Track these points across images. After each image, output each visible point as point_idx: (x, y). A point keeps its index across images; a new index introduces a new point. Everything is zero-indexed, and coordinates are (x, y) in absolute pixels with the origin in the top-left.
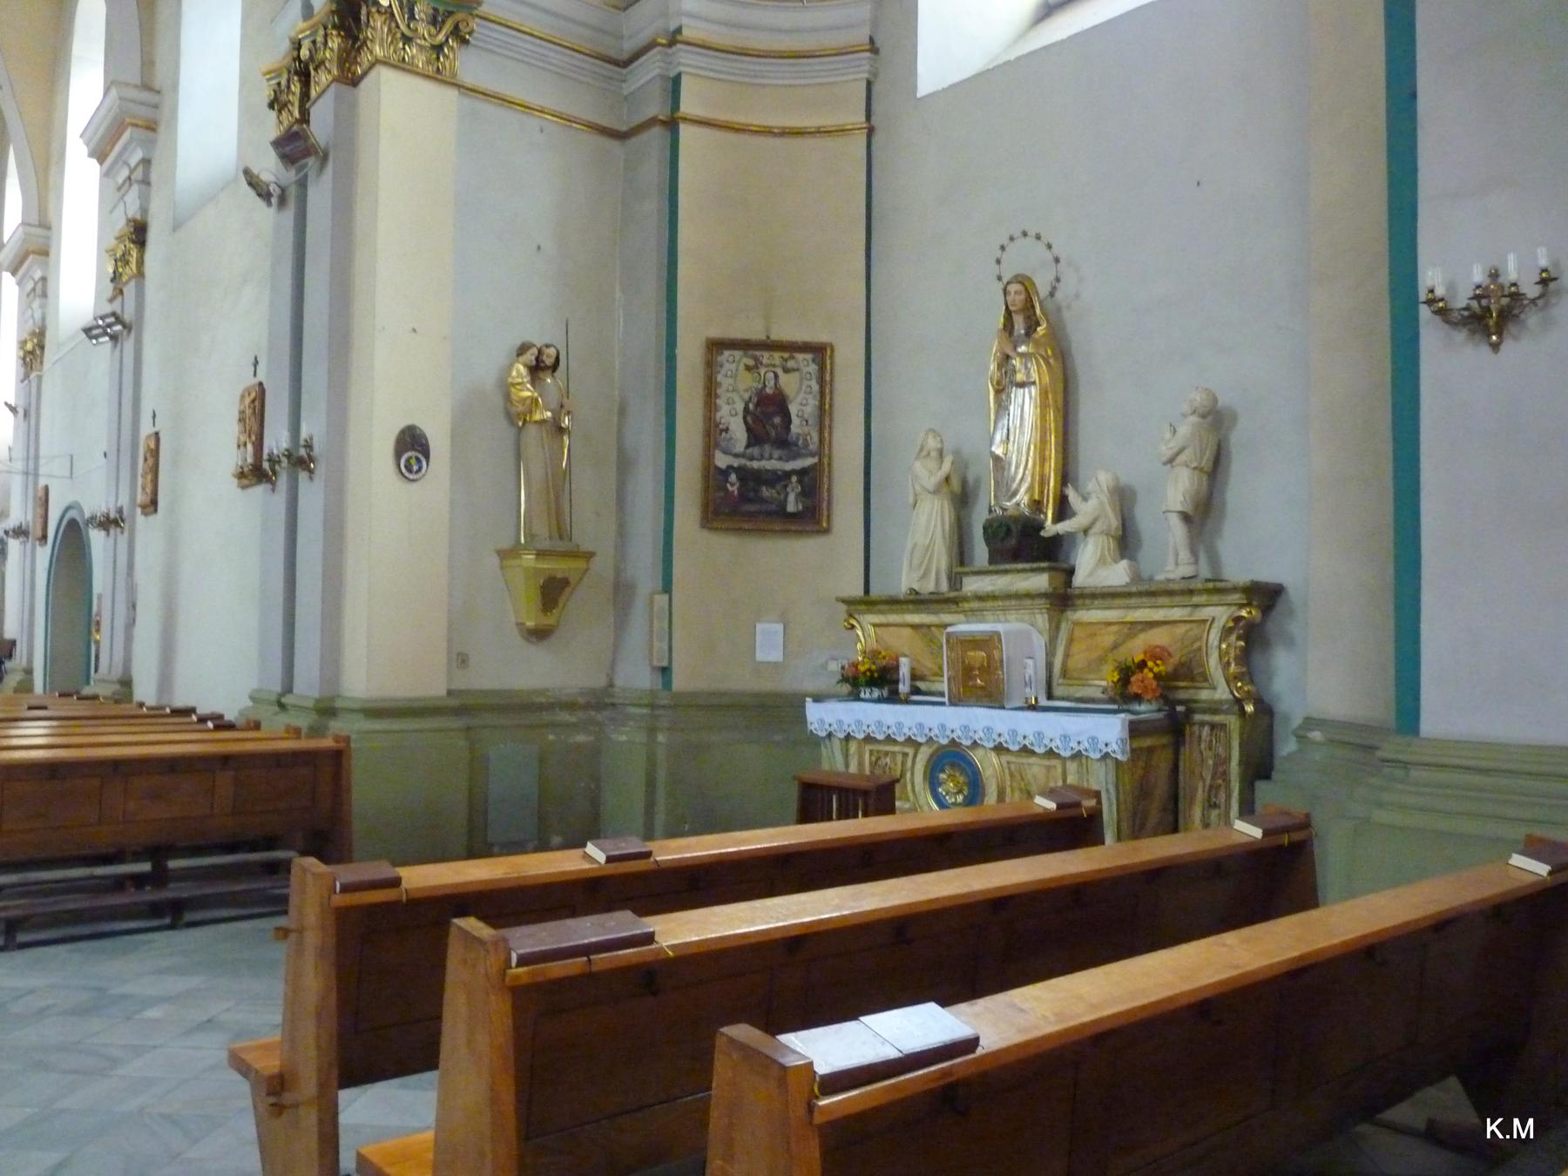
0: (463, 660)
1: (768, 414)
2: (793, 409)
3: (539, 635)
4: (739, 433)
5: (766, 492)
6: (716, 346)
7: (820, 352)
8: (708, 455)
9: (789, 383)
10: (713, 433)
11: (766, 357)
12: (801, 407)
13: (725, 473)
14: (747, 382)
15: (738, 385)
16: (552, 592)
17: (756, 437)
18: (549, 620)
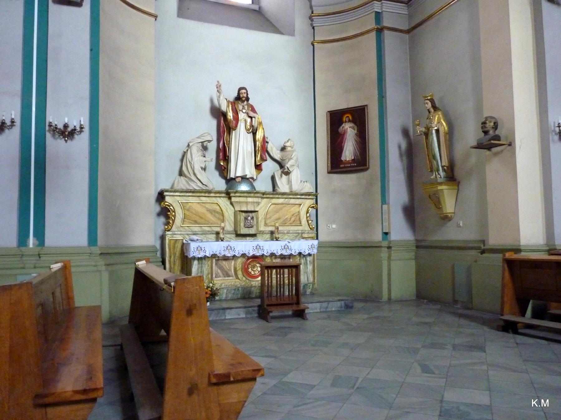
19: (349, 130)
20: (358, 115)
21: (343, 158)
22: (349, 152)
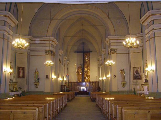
0: (119, 89)
1: (137, 72)
2: (139, 71)
3: (123, 87)
4: (135, 73)
5: (137, 77)
6: (133, 68)
7: (140, 67)
8: (133, 75)
9: (138, 70)
10: (134, 74)
11: (137, 68)
12: (139, 71)
13: (134, 76)
14: (135, 70)
15: (135, 70)
16: (124, 84)
17: (136, 74)
18: (124, 86)
19: (21, 71)
20: (23, 68)
21: (20, 76)
22: (21, 75)
